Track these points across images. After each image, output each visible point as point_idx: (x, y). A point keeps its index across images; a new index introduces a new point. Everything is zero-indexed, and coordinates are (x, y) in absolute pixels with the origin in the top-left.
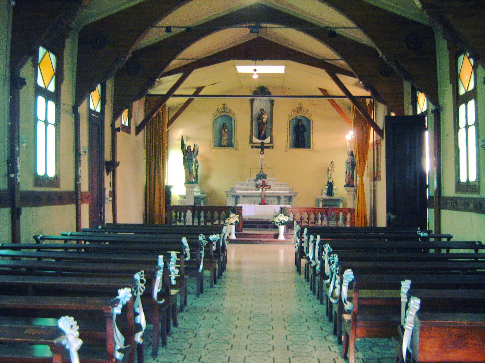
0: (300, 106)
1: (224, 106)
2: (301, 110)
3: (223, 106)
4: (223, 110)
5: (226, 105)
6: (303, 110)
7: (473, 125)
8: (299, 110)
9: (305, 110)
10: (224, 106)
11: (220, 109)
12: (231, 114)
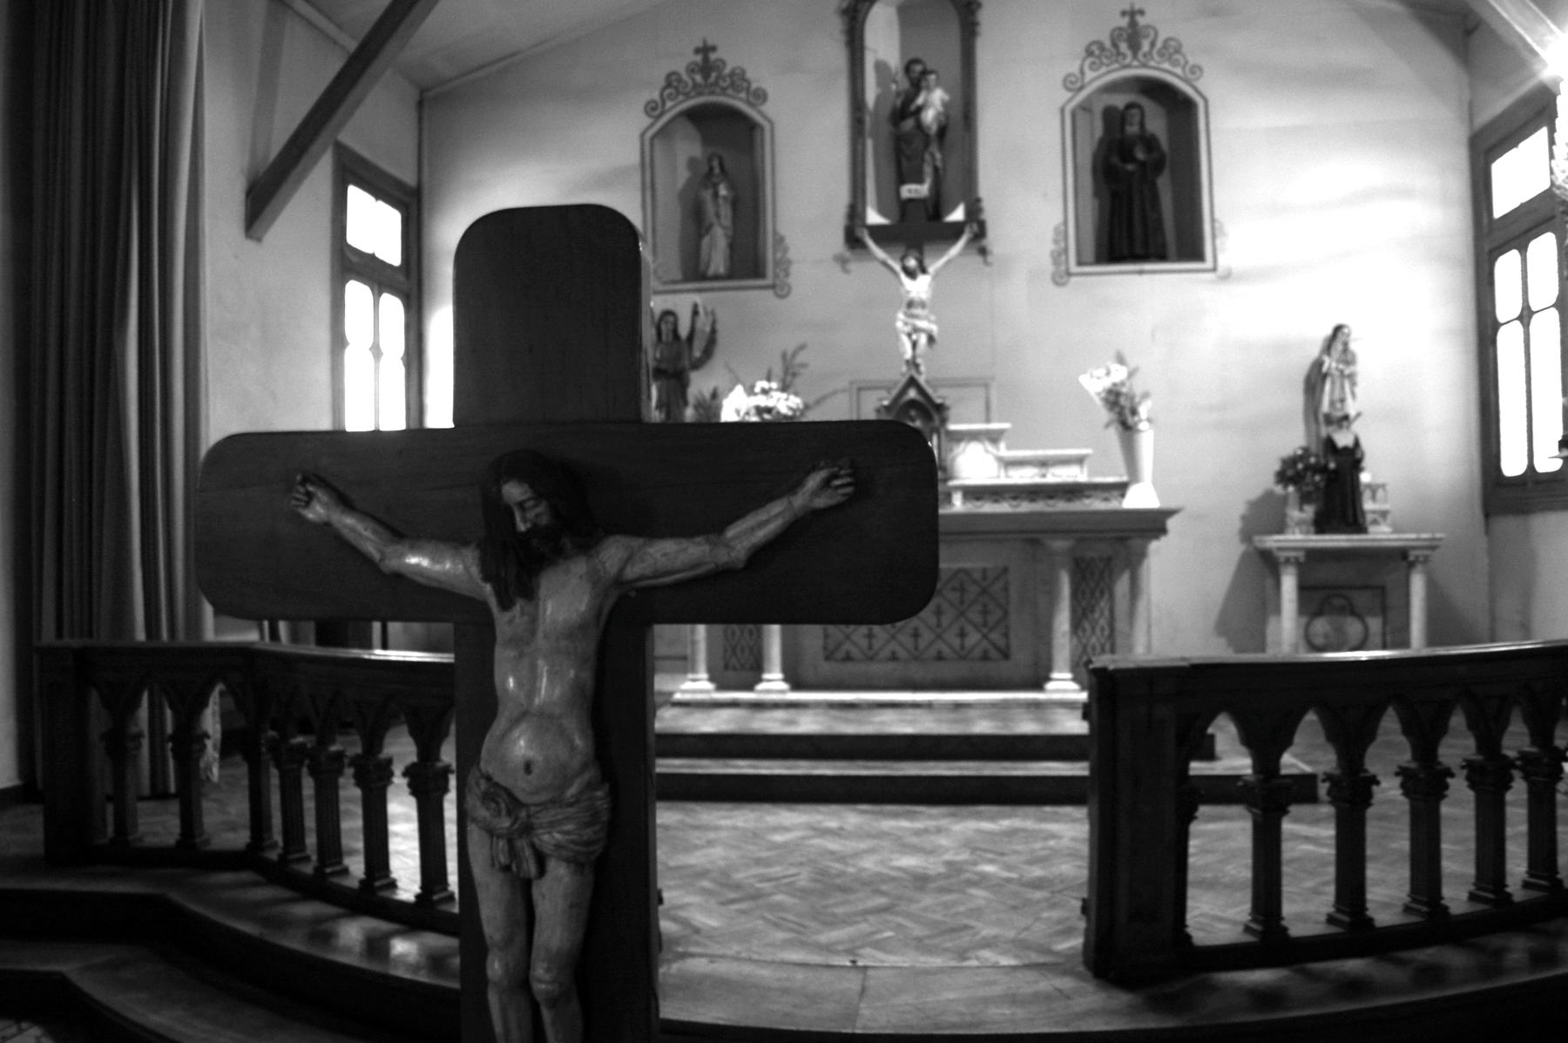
0: (1133, 24)
1: (706, 59)
2: (1135, 47)
3: (699, 58)
4: (698, 78)
5: (714, 49)
6: (1146, 46)
7: (1516, 319)
8: (1123, 47)
9: (1159, 44)
10: (706, 59)
11: (685, 77)
12: (743, 95)
